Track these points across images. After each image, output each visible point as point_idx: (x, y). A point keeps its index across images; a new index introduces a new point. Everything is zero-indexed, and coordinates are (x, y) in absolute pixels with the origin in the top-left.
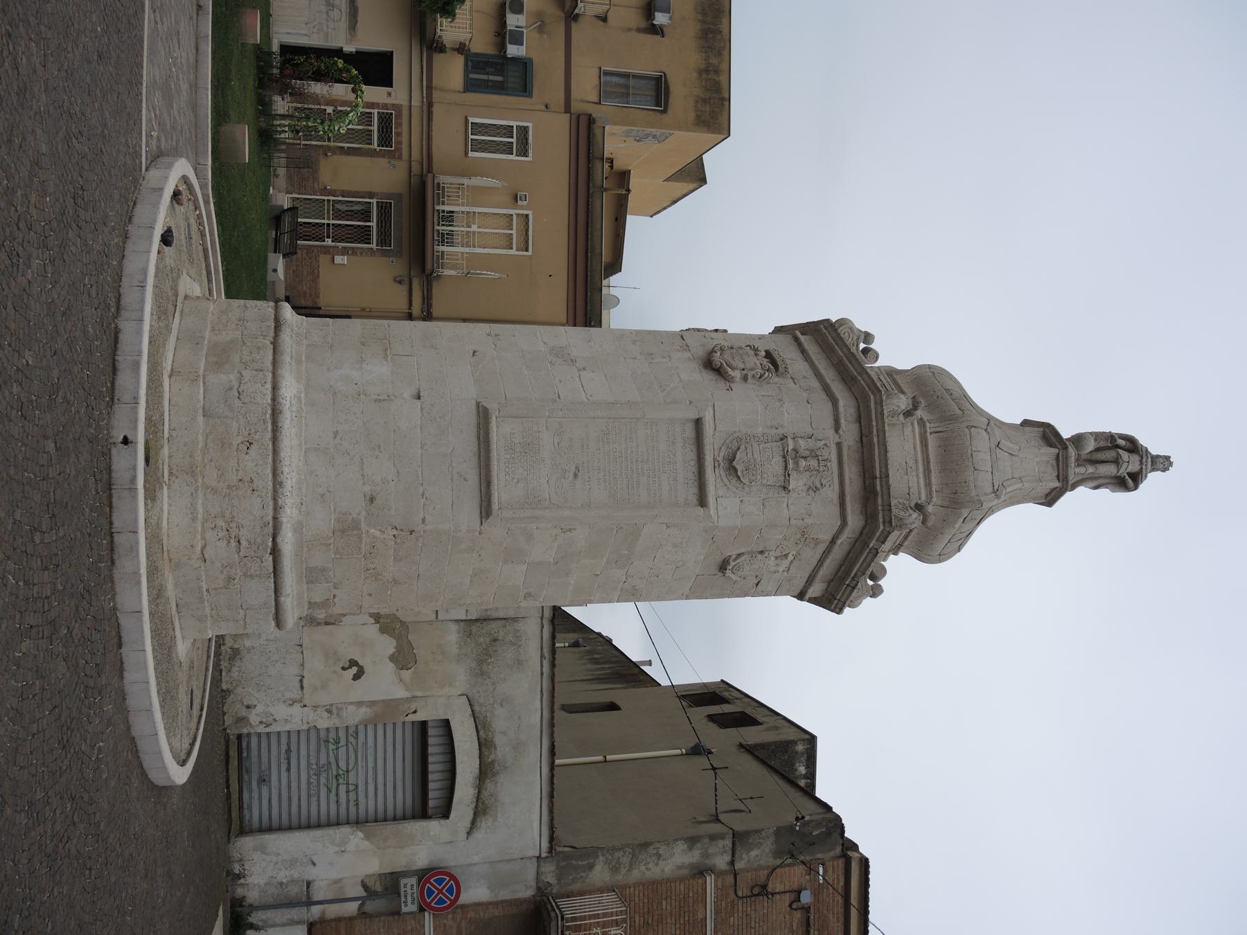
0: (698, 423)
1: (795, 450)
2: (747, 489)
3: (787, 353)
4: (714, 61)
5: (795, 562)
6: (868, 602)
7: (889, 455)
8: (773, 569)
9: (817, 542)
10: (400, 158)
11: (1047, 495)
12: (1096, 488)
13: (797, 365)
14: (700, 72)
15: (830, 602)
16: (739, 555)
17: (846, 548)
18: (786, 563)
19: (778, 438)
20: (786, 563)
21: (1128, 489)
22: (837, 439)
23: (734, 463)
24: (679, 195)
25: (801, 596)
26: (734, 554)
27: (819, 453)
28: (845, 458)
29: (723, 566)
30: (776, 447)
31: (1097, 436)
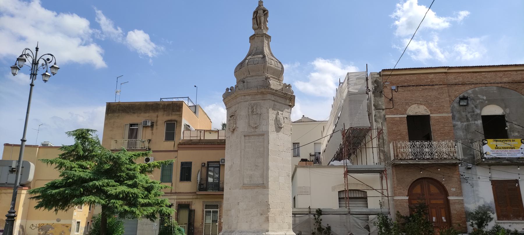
4: (161, 106)
6: (292, 89)
10: (192, 202)
14: (165, 111)
21: (268, 12)
24: (203, 112)
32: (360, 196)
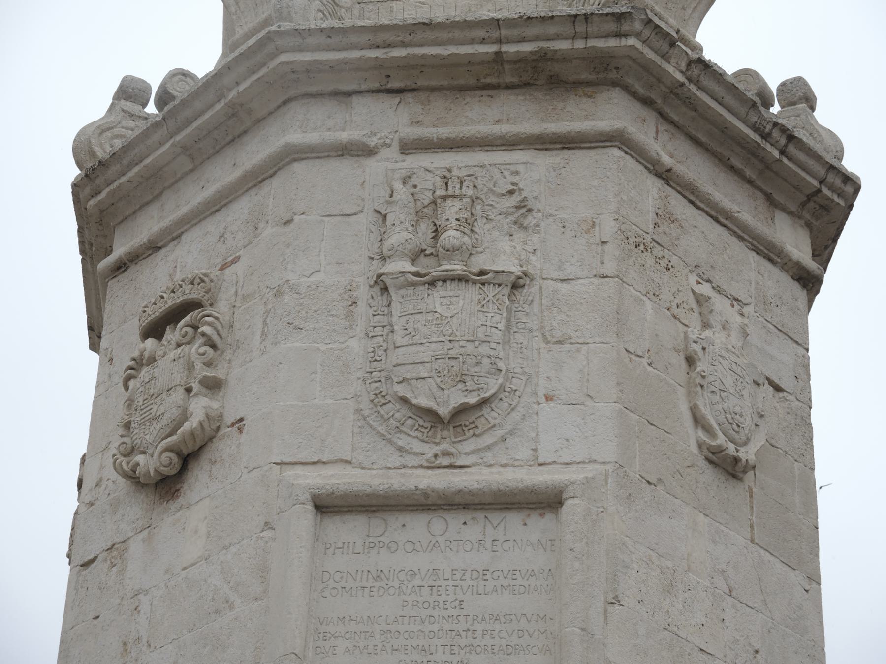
0: (326, 506)
1: (416, 255)
2: (516, 384)
3: (152, 286)
5: (719, 278)
6: (823, 116)
7: (439, 15)
8: (735, 339)
9: (663, 217)
13: (189, 258)
15: (826, 207)
16: (698, 420)
17: (683, 147)
18: (720, 304)
19: (380, 301)
20: (720, 304)
22: (393, 152)
23: (444, 411)
25: (810, 283)
26: (692, 436)
27: (427, 198)
28: (444, 132)
29: (730, 468)
30: (402, 303)
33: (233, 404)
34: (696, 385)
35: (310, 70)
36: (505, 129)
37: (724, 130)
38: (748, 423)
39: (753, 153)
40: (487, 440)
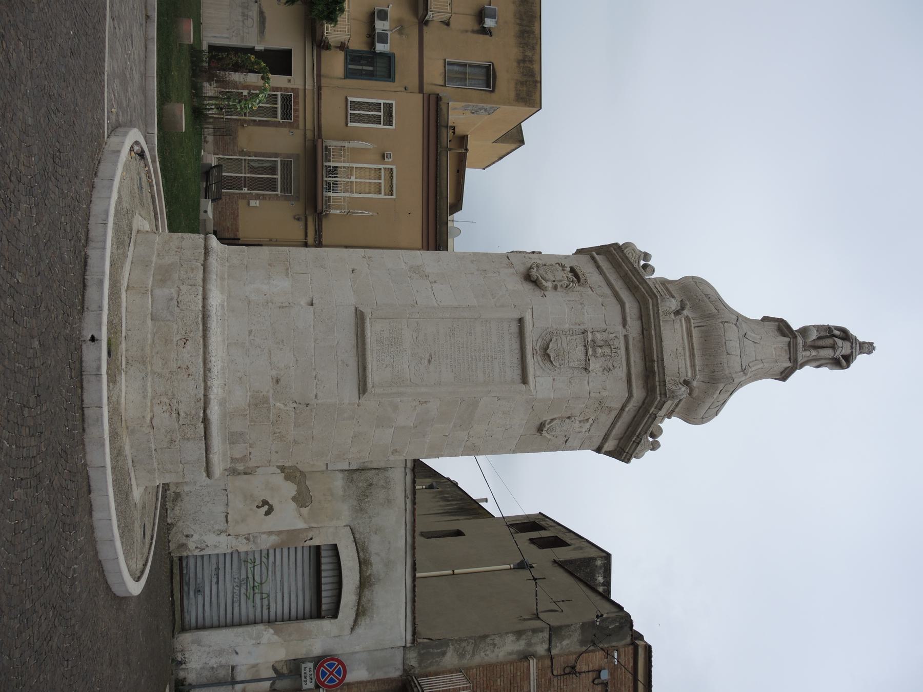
0: (521, 321)
2: (557, 370)
3: (586, 268)
4: (529, 53)
5: (595, 425)
6: (649, 454)
8: (577, 430)
9: (610, 409)
11: (782, 373)
12: (818, 367)
14: (519, 62)
16: (552, 420)
17: (632, 414)
18: (587, 425)
20: (587, 425)
21: (842, 368)
22: (624, 332)
25: (599, 450)
28: (631, 347)
29: (540, 428)
30: (579, 338)
31: (819, 328)
32: (324, 601)
33: (550, 294)
34: (562, 419)
35: (648, 308)
36: (632, 364)
37: (639, 425)
38: (553, 433)
39: (633, 433)
40: (541, 364)
